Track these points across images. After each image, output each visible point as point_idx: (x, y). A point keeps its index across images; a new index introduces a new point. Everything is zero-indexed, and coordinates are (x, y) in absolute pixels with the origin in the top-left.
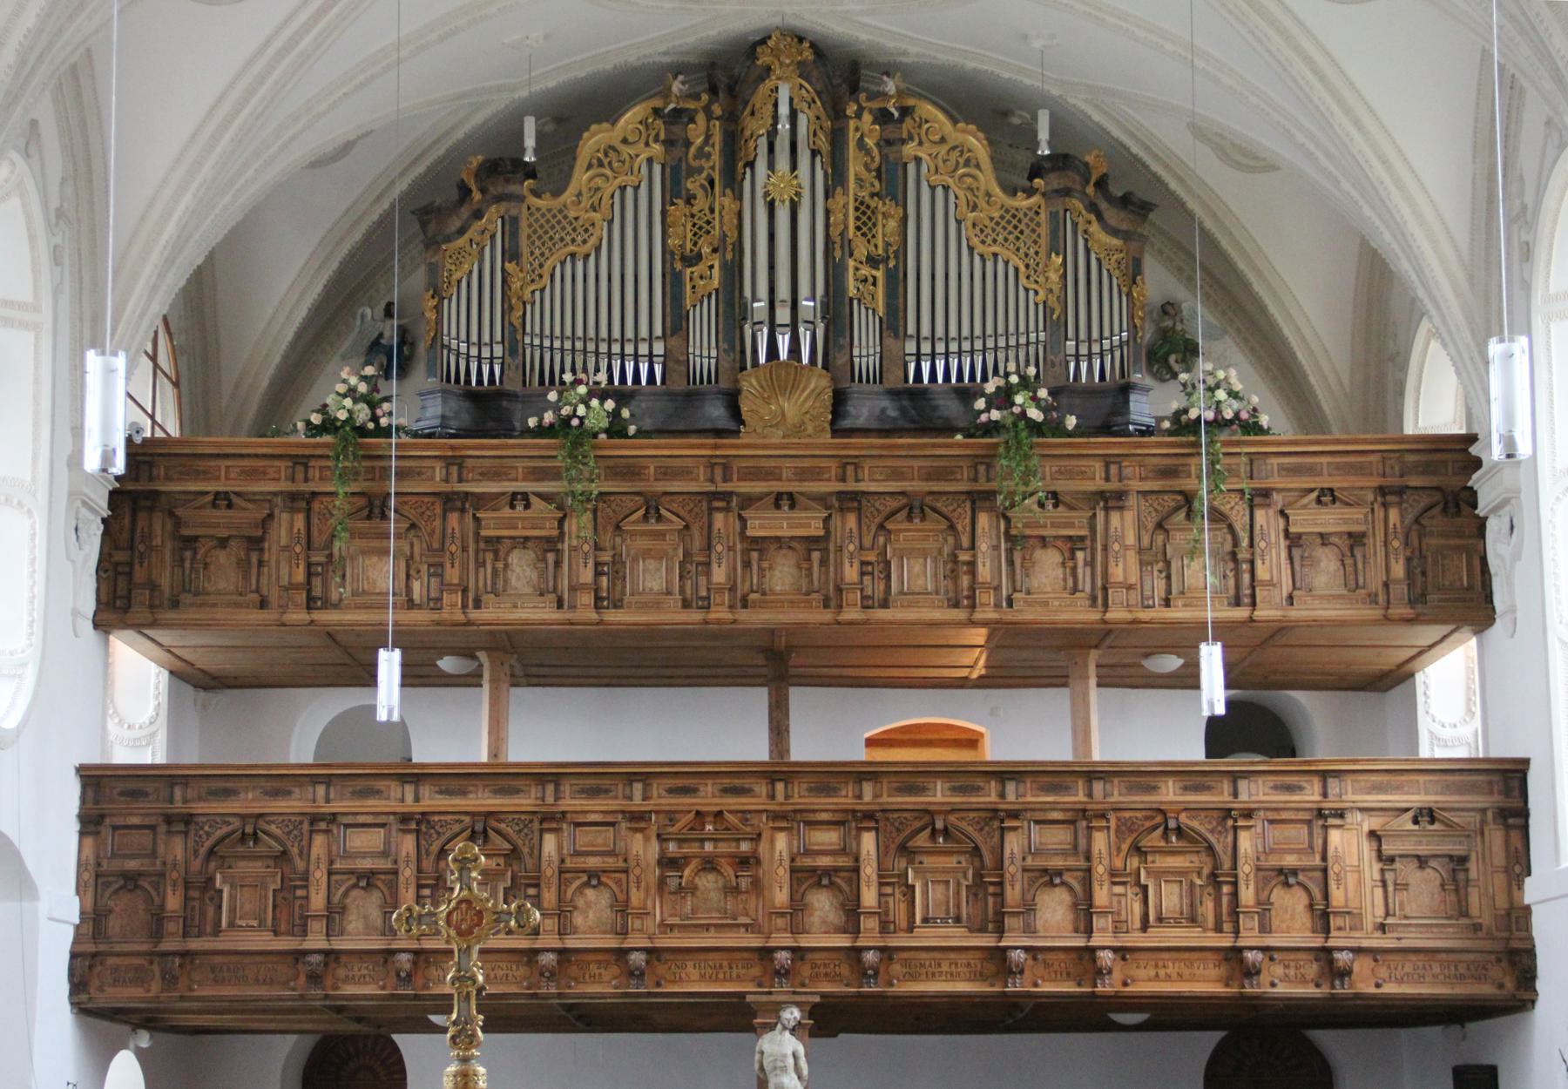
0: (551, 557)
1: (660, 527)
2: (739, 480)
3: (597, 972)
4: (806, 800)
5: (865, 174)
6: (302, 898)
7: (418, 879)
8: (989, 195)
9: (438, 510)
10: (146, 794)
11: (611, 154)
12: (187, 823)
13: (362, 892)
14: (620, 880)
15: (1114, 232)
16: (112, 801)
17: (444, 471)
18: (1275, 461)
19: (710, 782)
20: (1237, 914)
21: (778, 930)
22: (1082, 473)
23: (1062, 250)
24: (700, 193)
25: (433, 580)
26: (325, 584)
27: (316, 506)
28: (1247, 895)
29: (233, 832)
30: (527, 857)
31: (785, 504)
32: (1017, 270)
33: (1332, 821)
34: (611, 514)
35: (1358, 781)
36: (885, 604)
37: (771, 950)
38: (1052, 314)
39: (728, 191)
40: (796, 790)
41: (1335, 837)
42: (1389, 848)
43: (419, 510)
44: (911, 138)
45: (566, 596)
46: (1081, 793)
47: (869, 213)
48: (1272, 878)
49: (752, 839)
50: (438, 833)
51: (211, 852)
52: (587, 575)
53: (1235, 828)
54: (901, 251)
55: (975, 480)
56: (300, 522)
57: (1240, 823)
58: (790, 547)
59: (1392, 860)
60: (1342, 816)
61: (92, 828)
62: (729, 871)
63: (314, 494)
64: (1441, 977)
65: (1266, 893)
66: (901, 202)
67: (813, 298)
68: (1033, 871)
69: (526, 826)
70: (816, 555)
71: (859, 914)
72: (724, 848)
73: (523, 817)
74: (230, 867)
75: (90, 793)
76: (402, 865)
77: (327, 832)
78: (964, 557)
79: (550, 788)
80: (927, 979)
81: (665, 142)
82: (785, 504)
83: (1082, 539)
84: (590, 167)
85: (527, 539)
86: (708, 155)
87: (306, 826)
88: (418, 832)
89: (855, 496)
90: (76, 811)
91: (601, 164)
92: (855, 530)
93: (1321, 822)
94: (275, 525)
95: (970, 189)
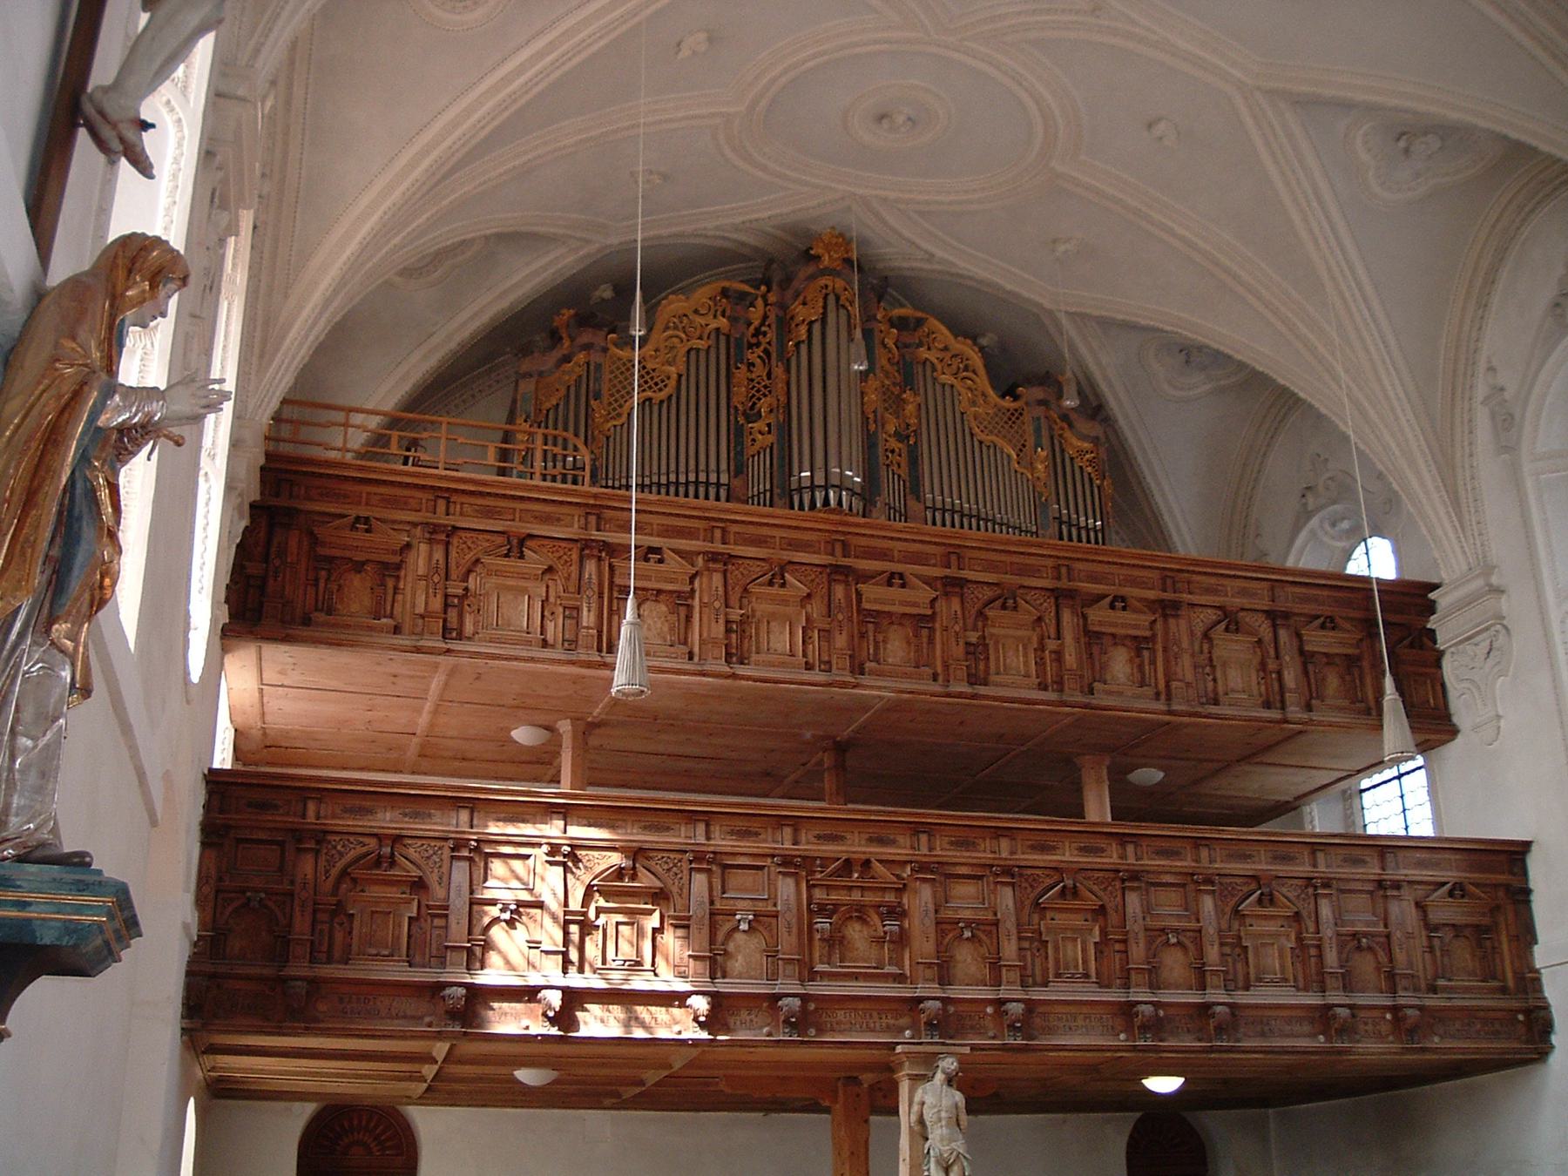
1: (782, 591)
3: (748, 1018)
4: (950, 853)
5: (888, 367)
6: (441, 927)
8: (983, 394)
9: (575, 556)
10: (276, 807)
11: (685, 320)
15: (1084, 438)
17: (583, 520)
18: (1291, 589)
21: (926, 980)
22: (1144, 582)
25: (568, 622)
26: (461, 616)
27: (455, 541)
30: (676, 896)
31: (897, 581)
32: (1009, 456)
34: (740, 576)
38: (1040, 498)
40: (938, 843)
41: (1395, 909)
42: (1436, 916)
43: (557, 555)
44: (920, 345)
49: (897, 889)
51: (344, 873)
53: (1316, 896)
55: (1059, 578)
56: (439, 555)
58: (900, 624)
59: (1436, 928)
63: (455, 528)
72: (870, 898)
74: (363, 891)
79: (701, 828)
81: (729, 318)
82: (897, 581)
84: (667, 328)
85: (659, 592)
86: (765, 334)
87: (447, 853)
89: (961, 583)
91: (676, 328)
93: (1381, 893)
95: (970, 389)
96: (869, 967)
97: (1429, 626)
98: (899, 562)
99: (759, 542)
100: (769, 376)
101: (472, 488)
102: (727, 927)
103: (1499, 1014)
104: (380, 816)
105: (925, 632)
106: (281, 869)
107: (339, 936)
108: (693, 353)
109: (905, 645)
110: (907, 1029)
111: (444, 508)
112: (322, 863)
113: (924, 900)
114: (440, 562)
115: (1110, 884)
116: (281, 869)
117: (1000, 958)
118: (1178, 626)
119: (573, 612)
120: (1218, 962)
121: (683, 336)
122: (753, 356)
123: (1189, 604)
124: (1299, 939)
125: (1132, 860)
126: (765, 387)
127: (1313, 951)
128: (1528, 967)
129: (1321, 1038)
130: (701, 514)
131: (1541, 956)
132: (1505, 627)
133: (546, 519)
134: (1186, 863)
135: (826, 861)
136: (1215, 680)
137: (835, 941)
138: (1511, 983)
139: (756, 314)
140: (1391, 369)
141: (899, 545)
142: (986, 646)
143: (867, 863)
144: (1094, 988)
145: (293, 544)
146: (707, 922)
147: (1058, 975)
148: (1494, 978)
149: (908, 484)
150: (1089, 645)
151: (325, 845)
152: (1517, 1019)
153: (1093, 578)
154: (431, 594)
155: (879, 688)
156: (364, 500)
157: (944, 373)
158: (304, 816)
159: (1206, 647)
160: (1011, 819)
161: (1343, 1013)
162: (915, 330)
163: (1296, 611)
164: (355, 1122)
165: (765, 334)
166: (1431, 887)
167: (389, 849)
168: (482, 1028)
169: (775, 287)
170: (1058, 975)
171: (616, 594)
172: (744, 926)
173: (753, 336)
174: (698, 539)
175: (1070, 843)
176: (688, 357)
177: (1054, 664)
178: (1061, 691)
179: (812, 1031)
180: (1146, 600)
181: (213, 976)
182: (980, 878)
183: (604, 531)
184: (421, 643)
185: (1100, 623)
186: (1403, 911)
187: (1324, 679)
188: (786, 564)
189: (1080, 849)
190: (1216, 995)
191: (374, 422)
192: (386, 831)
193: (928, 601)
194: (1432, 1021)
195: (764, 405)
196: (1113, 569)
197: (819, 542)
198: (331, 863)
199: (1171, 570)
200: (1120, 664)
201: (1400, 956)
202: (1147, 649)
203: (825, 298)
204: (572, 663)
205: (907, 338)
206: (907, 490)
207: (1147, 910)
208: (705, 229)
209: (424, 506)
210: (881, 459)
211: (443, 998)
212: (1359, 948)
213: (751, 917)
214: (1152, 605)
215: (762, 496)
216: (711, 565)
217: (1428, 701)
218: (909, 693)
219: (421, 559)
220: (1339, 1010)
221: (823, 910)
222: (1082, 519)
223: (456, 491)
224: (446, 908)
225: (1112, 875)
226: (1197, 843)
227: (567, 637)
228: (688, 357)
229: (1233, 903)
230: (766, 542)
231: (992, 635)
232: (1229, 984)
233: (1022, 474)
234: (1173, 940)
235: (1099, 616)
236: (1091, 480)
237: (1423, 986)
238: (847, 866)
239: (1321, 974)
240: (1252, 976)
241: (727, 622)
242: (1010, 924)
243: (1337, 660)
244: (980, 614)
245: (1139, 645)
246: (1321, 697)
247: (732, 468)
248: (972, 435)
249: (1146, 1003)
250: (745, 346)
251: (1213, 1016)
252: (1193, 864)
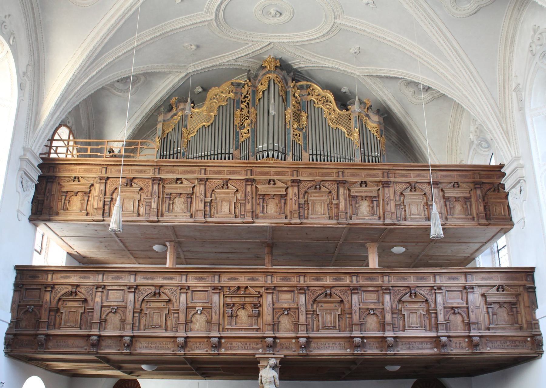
2: (256, 175)
8: (334, 110)
9: (151, 184)
11: (218, 96)
12: (52, 288)
13: (113, 314)
14: (209, 312)
15: (374, 122)
16: (26, 279)
17: (153, 171)
19: (243, 276)
20: (438, 324)
21: (268, 330)
24: (245, 108)
25: (147, 207)
27: (109, 182)
28: (441, 318)
30: (175, 303)
32: (344, 132)
33: (469, 290)
34: (211, 186)
35: (478, 276)
36: (405, 219)
39: (253, 108)
41: (471, 297)
42: (489, 300)
43: (144, 184)
45: (194, 214)
47: (297, 115)
48: (449, 311)
49: (258, 297)
50: (142, 293)
51: (60, 299)
52: (202, 206)
53: (435, 293)
54: (307, 126)
55: (339, 176)
57: (437, 291)
60: (473, 289)
61: (18, 289)
64: (510, 346)
65: (447, 317)
66: (307, 112)
67: (282, 146)
68: (363, 309)
73: (174, 288)
75: (19, 276)
76: (128, 305)
77: (102, 292)
78: (335, 202)
80: (324, 349)
84: (211, 99)
85: (181, 194)
86: (248, 97)
88: (135, 292)
90: (13, 282)
93: (465, 291)
97: (502, 182)
100: (248, 112)
102: (193, 312)
103: (519, 338)
104: (72, 278)
105: (283, 201)
106: (40, 297)
107: (58, 320)
108: (221, 107)
110: (260, 348)
112: (53, 295)
119: (149, 203)
120: (390, 321)
121: (216, 101)
122: (243, 106)
126: (247, 116)
127: (433, 315)
128: (533, 318)
129: (436, 349)
131: (539, 314)
132: (524, 180)
133: (140, 172)
134: (379, 282)
136: (405, 211)
138: (525, 325)
139: (244, 91)
141: (274, 169)
142: (308, 204)
143: (247, 287)
147: (323, 327)
148: (517, 323)
149: (302, 146)
150: (445, 202)
152: (527, 340)
153: (353, 175)
157: (318, 104)
160: (306, 269)
161: (42, 337)
164: (130, 385)
165: (248, 97)
166: (490, 288)
167: (75, 290)
168: (136, 350)
172: (199, 312)
177: (336, 209)
178: (338, 219)
181: (15, 335)
182: (292, 291)
186: (475, 298)
187: (454, 207)
188: (228, 180)
195: (246, 123)
203: (269, 81)
208: (223, 62)
210: (292, 138)
211: (266, 342)
213: (202, 309)
215: (245, 156)
216: (200, 183)
217: (502, 213)
220: (442, 338)
221: (228, 305)
222: (373, 153)
223: (108, 165)
224: (93, 309)
229: (400, 296)
230: (221, 173)
231: (310, 200)
232: (394, 328)
234: (372, 313)
235: (355, 190)
236: (377, 138)
237: (483, 327)
239: (437, 324)
240: (320, 326)
241: (299, 204)
242: (303, 309)
243: (460, 199)
245: (372, 199)
247: (234, 147)
248: (329, 126)
252: (382, 283)
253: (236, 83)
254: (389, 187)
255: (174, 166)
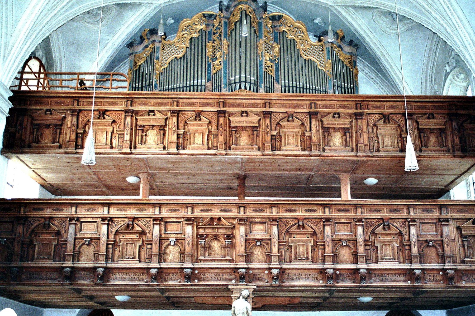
0: (162, 132)
1: (200, 122)
7: (107, 241)
9: (123, 116)
17: (126, 103)
21: (241, 261)
23: (331, 59)
29: (42, 223)
31: (244, 115)
33: (443, 223)
37: (238, 269)
39: (225, 39)
40: (248, 210)
41: (445, 230)
46: (353, 212)
49: (231, 228)
50: (116, 225)
51: (33, 231)
52: (174, 138)
53: (409, 225)
54: (279, 58)
55: (311, 108)
56: (75, 120)
58: (246, 130)
59: (466, 237)
62: (222, 239)
69: (148, 223)
70: (255, 133)
71: (271, 256)
79: (157, 209)
82: (244, 115)
83: (348, 129)
84: (183, 31)
85: (154, 126)
86: (220, 29)
87: (68, 222)
89: (270, 113)
92: (269, 124)
94: (66, 120)
96: (219, 257)
98: (246, 107)
99: (192, 105)
101: (86, 96)
102: (166, 244)
106: (12, 230)
107: (31, 252)
108: (193, 40)
109: (247, 138)
110: (233, 279)
111: (77, 104)
113: (241, 231)
114: (269, 124)
115: (318, 223)
116: (12, 230)
117: (184, 252)
118: (362, 123)
123: (367, 114)
124: (401, 243)
125: (327, 213)
126: (219, 48)
129: (409, 282)
130: (168, 97)
133: (113, 104)
135: (203, 219)
136: (378, 143)
137: (207, 248)
140: (452, 10)
142: (280, 136)
143: (219, 219)
144: (311, 263)
145: (26, 120)
146: (158, 242)
147: (296, 258)
149: (275, 78)
151: (27, 221)
153: (326, 107)
154: (71, 134)
155: (236, 154)
156: (49, 104)
158: (20, 212)
159: (375, 130)
161: (418, 272)
162: (279, 20)
163: (416, 113)
169: (223, 11)
170: (296, 258)
171: (138, 128)
172: (172, 243)
173: (216, 30)
174: (168, 106)
175: (367, 208)
176: (191, 41)
178: (311, 151)
179: (196, 281)
180: (348, 113)
182: (265, 223)
183: (134, 106)
184: (67, 151)
185: (328, 124)
189: (306, 210)
190: (362, 265)
191: (94, 77)
192: (47, 216)
193: (257, 121)
194: (461, 275)
195: (218, 54)
196: (335, 102)
197: (214, 103)
198: (29, 227)
199: (359, 101)
200: (337, 139)
201: (447, 249)
202: (348, 132)
204: (121, 153)
205: (276, 23)
206: (274, 80)
207: (333, 233)
209: (70, 103)
210: (264, 70)
211: (238, 272)
212: (428, 246)
214: (350, 115)
215: (218, 88)
216: (173, 115)
218: (247, 155)
219: (70, 121)
223: (81, 97)
224: (66, 241)
225: (319, 220)
226: (408, 207)
227: (119, 144)
228: (191, 41)
232: (368, 260)
233: (322, 70)
234: (344, 244)
235: (328, 121)
236: (349, 69)
237: (458, 261)
238: (212, 220)
241: (178, 135)
242: (275, 240)
244: (278, 124)
245: (345, 131)
246: (426, 146)
249: (330, 269)
250: (212, 34)
251: (359, 273)
253: (208, 14)
254: (362, 119)
255: (146, 98)
